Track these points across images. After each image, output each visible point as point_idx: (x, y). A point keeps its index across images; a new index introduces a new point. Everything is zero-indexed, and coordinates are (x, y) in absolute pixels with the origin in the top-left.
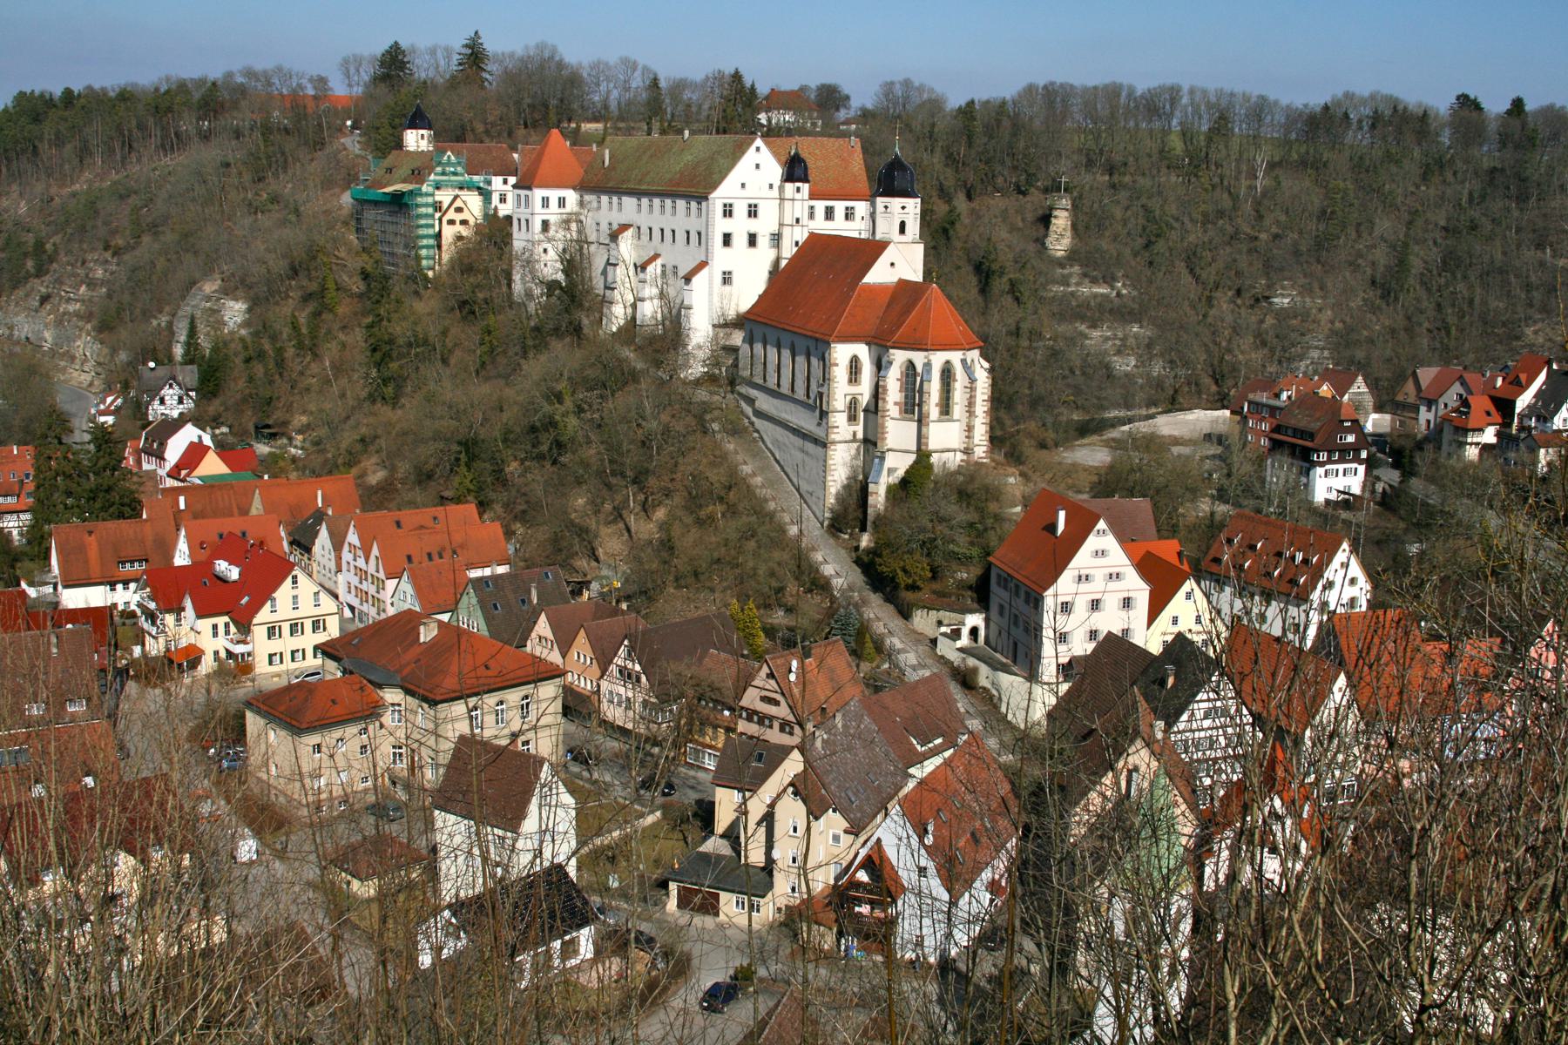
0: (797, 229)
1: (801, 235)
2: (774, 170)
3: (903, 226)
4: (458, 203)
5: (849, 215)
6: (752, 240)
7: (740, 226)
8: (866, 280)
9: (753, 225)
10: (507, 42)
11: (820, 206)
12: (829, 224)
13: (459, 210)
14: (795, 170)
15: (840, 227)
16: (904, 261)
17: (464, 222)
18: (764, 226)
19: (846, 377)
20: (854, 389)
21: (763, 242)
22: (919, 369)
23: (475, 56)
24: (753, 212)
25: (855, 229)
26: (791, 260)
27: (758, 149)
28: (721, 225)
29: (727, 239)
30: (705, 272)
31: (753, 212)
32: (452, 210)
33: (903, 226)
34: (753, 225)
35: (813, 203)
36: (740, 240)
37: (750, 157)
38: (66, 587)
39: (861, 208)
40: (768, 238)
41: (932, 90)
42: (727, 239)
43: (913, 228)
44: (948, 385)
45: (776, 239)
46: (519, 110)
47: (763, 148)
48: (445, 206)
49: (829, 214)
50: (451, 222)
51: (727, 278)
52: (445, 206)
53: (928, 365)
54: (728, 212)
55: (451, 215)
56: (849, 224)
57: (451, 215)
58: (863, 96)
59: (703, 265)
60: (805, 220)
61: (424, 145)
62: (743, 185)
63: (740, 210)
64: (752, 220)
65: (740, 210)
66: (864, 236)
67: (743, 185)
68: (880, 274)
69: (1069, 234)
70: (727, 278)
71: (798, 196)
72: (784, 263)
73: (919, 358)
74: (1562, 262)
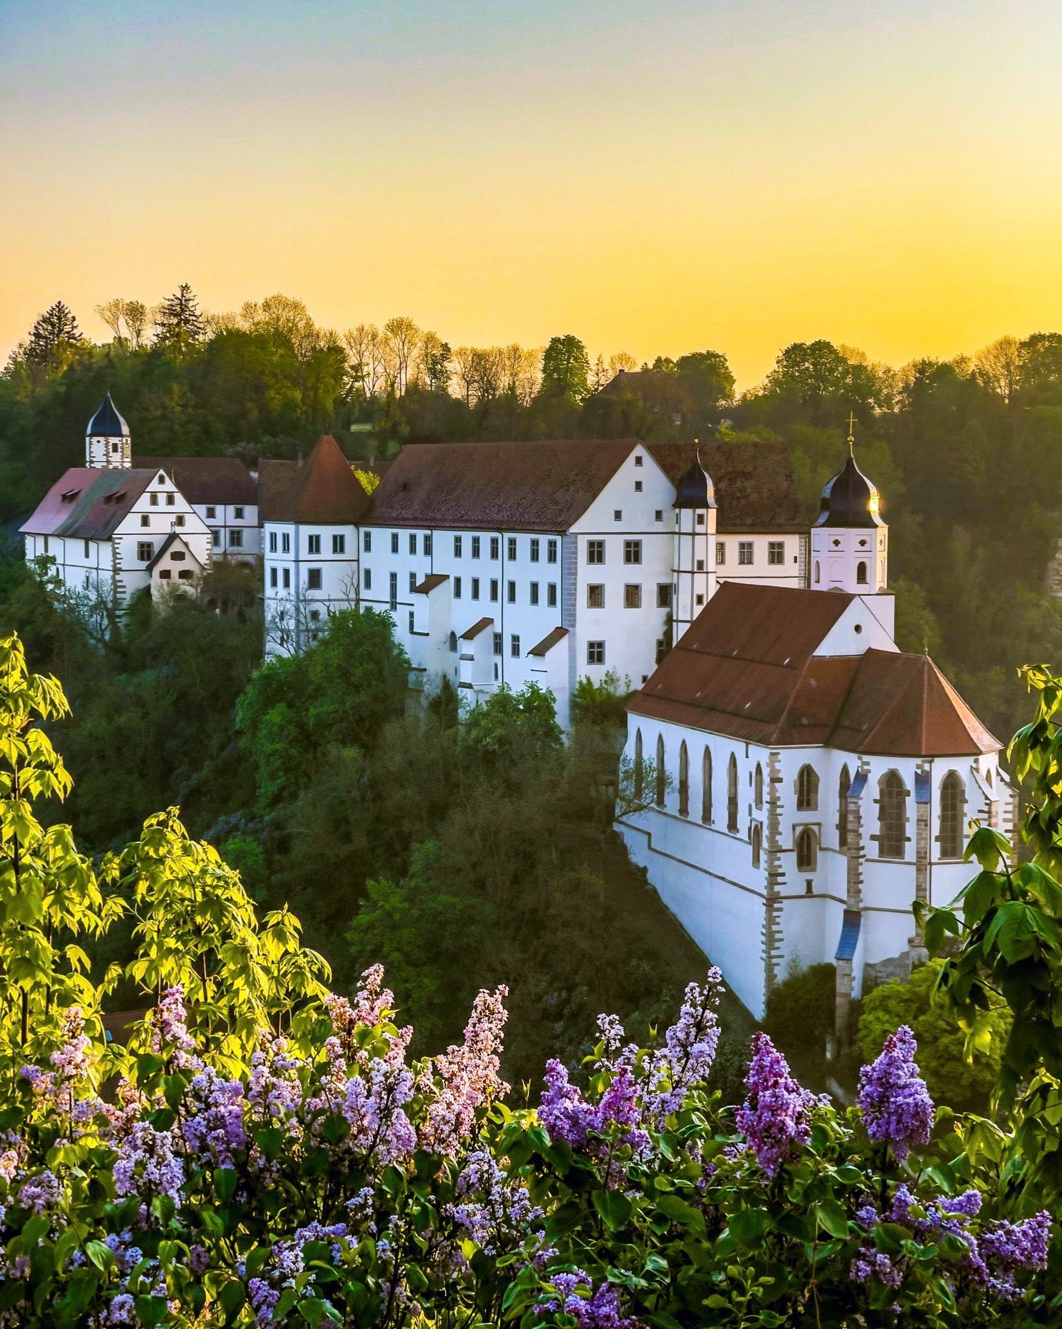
1: (708, 587)
3: (862, 569)
4: (176, 547)
5: (776, 555)
6: (632, 595)
7: (614, 574)
8: (819, 652)
9: (633, 574)
11: (732, 543)
12: (746, 570)
15: (761, 572)
17: (184, 574)
18: (648, 575)
20: (807, 817)
21: (649, 596)
22: (909, 784)
24: (633, 553)
25: (787, 576)
26: (695, 625)
27: (639, 461)
28: (587, 574)
31: (633, 553)
32: (167, 555)
33: (862, 569)
34: (633, 574)
35: (722, 538)
36: (614, 595)
37: (628, 472)
38: (846, 912)
39: (792, 544)
40: (655, 589)
42: (596, 595)
43: (879, 575)
44: (954, 807)
45: (665, 594)
47: (648, 460)
49: (746, 556)
50: (165, 574)
52: (156, 549)
53: (923, 780)
54: (596, 553)
56: (776, 569)
57: (166, 563)
59: (559, 633)
60: (711, 565)
61: (122, 460)
62: (618, 515)
63: (614, 549)
65: (614, 549)
66: (795, 584)
67: (618, 515)
68: (839, 642)
72: (680, 631)
73: (907, 768)
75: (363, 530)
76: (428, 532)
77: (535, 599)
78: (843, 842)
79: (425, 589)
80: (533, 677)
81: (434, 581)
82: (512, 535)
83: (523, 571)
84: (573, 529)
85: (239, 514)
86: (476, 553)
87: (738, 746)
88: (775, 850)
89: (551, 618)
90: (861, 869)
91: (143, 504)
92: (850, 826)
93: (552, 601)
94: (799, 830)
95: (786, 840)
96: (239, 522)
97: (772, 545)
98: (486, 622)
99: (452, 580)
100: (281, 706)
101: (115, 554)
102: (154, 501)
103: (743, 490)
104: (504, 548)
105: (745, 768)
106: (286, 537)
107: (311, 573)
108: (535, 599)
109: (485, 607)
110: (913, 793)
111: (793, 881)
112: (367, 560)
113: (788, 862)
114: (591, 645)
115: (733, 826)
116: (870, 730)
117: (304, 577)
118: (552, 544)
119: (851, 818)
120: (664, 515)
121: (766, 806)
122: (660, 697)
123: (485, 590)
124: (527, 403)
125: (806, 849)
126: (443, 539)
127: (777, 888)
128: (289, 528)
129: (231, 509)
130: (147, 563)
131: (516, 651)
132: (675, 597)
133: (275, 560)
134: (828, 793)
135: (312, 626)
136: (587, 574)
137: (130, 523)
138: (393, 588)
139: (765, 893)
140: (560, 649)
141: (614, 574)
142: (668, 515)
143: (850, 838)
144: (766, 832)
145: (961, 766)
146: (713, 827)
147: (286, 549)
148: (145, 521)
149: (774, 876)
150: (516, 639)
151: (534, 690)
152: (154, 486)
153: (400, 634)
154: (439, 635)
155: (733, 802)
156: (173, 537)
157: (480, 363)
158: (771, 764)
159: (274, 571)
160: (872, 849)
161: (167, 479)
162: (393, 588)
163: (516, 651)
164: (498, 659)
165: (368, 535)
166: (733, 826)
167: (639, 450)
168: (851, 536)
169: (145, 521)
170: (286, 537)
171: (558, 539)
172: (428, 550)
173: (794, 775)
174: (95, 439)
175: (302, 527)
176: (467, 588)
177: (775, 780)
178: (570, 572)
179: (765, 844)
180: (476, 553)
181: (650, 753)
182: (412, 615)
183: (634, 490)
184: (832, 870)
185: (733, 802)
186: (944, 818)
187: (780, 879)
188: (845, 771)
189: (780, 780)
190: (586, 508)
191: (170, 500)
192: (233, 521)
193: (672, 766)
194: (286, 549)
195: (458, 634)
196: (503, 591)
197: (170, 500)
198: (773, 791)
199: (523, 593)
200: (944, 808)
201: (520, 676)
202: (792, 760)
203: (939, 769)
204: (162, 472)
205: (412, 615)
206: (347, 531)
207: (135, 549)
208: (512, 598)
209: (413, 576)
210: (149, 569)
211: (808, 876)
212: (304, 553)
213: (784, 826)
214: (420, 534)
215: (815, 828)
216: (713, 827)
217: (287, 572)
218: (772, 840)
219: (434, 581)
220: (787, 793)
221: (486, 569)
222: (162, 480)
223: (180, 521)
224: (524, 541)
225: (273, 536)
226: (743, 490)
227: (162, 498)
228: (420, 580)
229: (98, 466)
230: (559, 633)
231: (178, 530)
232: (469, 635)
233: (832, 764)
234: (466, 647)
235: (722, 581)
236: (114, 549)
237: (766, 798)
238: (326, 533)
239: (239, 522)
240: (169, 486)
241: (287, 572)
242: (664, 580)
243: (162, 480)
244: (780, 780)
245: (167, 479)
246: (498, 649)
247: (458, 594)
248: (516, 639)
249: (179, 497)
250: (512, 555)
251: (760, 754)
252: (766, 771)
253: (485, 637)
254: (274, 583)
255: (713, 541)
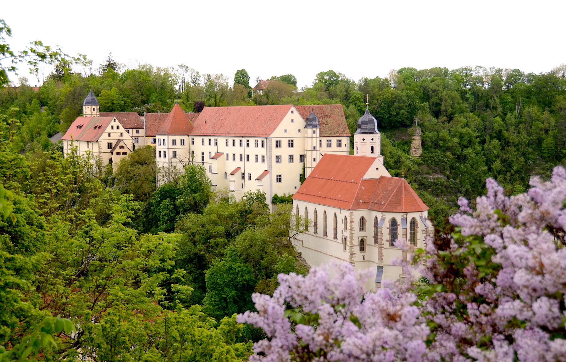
0: (314, 152)
2: (299, 121)
3: (372, 148)
5: (339, 144)
6: (291, 158)
7: (285, 151)
9: (291, 151)
10: (129, 62)
11: (324, 140)
12: (329, 149)
13: (122, 147)
14: (309, 122)
15: (334, 150)
16: (377, 170)
17: (124, 154)
18: (296, 152)
19: (359, 228)
20: (362, 234)
21: (297, 158)
22: (399, 221)
23: (111, 66)
24: (291, 144)
27: (292, 112)
29: (278, 159)
30: (268, 176)
31: (291, 144)
32: (118, 147)
33: (372, 148)
37: (289, 116)
41: (344, 76)
42: (278, 159)
44: (414, 230)
46: (140, 96)
47: (296, 112)
48: (113, 145)
49: (329, 144)
50: (118, 154)
51: (279, 179)
53: (383, 220)
54: (278, 144)
55: (118, 150)
56: (339, 149)
57: (118, 150)
58: (305, 81)
60: (318, 148)
62: (286, 131)
63: (285, 143)
64: (291, 149)
65: (285, 143)
67: (286, 131)
69: (421, 148)
70: (279, 179)
71: (314, 135)
73: (398, 217)
74: (564, 151)
75: (191, 137)
76: (216, 138)
77: (257, 160)
78: (376, 242)
79: (215, 158)
80: (258, 188)
81: (218, 155)
82: (248, 139)
83: (252, 151)
84: (271, 136)
85: (137, 132)
86: (234, 144)
87: (337, 211)
88: (353, 246)
89: (262, 167)
90: (383, 251)
91: (109, 129)
92: (379, 237)
93: (263, 161)
94: (360, 239)
95: (356, 242)
96: (137, 135)
97: (338, 140)
98: (238, 169)
99: (225, 155)
100: (168, 199)
101: (99, 147)
102: (112, 128)
103: (327, 122)
104: (245, 143)
105: (340, 218)
106: (164, 140)
107: (172, 154)
108: (257, 160)
109: (238, 163)
110: (401, 225)
111: (359, 255)
112: (193, 148)
113: (357, 249)
114: (277, 176)
115: (335, 237)
116: (385, 204)
117: (171, 155)
118: (263, 141)
119: (379, 234)
120: (301, 131)
121: (348, 231)
122: (304, 195)
123: (238, 157)
124: (232, 89)
125: (362, 245)
126: (221, 141)
127: (353, 259)
128: (165, 137)
129: (135, 130)
130: (110, 150)
131: (250, 178)
132: (305, 159)
133: (160, 148)
134: (370, 225)
135: (174, 171)
136: (276, 152)
137: (105, 136)
138: (203, 157)
139: (349, 260)
140: (266, 178)
141: (285, 151)
142: (303, 130)
143: (379, 241)
144: (348, 239)
145: (417, 216)
146: (327, 238)
147: (164, 144)
148: (109, 135)
149: (352, 254)
150: (250, 174)
151: (259, 192)
152: (112, 123)
153: (207, 173)
154: (221, 174)
155: (335, 229)
156: (119, 141)
157: (158, 69)
158: (350, 216)
159: (160, 152)
160: (387, 244)
161: (117, 120)
162: (203, 157)
163: (250, 178)
164: (243, 181)
165: (193, 139)
166: (335, 237)
167: (293, 109)
168: (368, 137)
169: (109, 135)
170: (164, 140)
171: (265, 140)
172: (216, 144)
173: (359, 220)
174: (87, 106)
175: (170, 137)
176: (231, 157)
177: (352, 222)
178: (270, 151)
179: (348, 244)
180: (234, 144)
181: (302, 213)
182: (210, 167)
183: (291, 122)
184: (373, 251)
185: (335, 229)
186: (411, 234)
187: (354, 255)
188: (376, 218)
189: (353, 222)
190: (275, 129)
191: (118, 128)
192: (135, 134)
193: (311, 217)
194: (164, 144)
195: (228, 174)
196: (245, 158)
197: (118, 128)
198: (351, 226)
199: (252, 158)
200: (411, 230)
201: (253, 187)
202: (358, 214)
203: (410, 217)
204: (115, 118)
205: (210, 167)
206: (185, 138)
207: (106, 145)
208: (248, 160)
209: (210, 153)
210: (112, 152)
211: (363, 254)
212: (171, 146)
213: (355, 237)
214: (213, 139)
215: (365, 238)
216: (327, 238)
217: (165, 152)
218: (351, 243)
219: (218, 155)
220: (356, 226)
221: (238, 150)
222: (115, 120)
223: (121, 135)
224: (252, 141)
225: (159, 140)
226: (327, 122)
227: (115, 127)
228: (213, 155)
229: (88, 116)
230: (266, 172)
231: (121, 138)
232: (232, 174)
233: (370, 216)
234: (231, 178)
235: (323, 154)
236: (99, 145)
237: (348, 227)
238: (178, 139)
239: (137, 135)
240: (117, 123)
241: (165, 152)
242: (302, 154)
243: (115, 120)
244: (353, 222)
245: (117, 120)
246: (243, 178)
247: (227, 159)
248: (250, 174)
249: (121, 127)
250: (248, 145)
251: (346, 213)
252: (348, 219)
253: (238, 175)
254: (160, 156)
255: (318, 139)
